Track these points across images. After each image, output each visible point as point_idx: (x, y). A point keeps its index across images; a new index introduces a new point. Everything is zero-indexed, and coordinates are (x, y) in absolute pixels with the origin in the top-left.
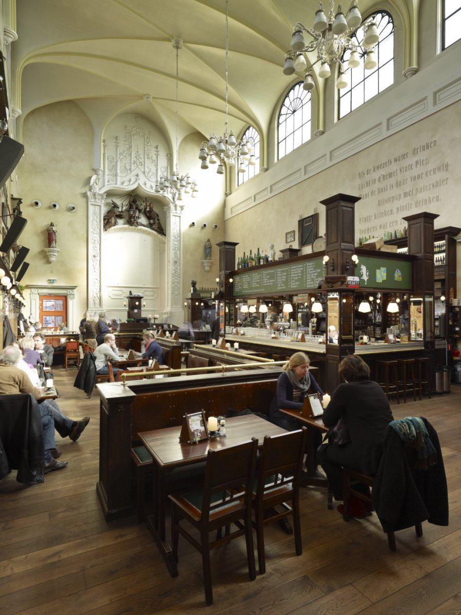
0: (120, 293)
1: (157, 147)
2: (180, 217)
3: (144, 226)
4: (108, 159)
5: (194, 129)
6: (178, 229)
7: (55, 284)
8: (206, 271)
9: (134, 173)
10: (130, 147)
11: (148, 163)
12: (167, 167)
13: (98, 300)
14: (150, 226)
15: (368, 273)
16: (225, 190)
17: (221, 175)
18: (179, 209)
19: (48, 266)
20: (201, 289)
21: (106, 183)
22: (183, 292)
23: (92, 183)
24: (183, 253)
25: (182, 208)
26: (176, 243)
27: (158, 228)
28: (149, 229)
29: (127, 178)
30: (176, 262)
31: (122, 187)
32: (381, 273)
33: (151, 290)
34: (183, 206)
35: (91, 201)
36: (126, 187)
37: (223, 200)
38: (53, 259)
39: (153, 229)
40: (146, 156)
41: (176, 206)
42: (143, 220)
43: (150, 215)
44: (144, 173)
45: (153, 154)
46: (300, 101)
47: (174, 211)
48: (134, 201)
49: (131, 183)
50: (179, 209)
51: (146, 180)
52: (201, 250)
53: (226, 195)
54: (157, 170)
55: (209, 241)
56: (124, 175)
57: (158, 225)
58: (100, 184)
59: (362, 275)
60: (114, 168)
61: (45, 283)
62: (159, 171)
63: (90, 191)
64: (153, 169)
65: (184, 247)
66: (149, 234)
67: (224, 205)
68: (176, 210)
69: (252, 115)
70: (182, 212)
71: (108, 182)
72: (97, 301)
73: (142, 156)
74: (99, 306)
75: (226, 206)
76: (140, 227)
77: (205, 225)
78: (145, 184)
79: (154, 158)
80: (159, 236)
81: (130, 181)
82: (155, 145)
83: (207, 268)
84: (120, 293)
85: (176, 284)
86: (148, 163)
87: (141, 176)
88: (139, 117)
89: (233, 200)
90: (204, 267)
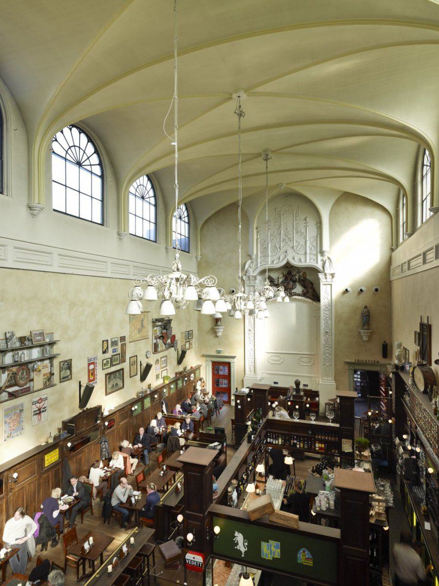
0: (278, 358)
1: (306, 219)
2: (331, 285)
3: (299, 295)
4: (260, 243)
5: (339, 191)
6: (330, 298)
7: (221, 354)
8: (364, 341)
9: (283, 250)
10: (280, 227)
11: (296, 237)
12: (317, 236)
13: (253, 367)
14: (304, 294)
15: (246, 544)
16: (391, 245)
17: (329, 257)
18: (329, 277)
19: (217, 339)
20: (357, 361)
21: (259, 265)
22: (335, 364)
23: (246, 268)
24: (335, 321)
25: (333, 275)
26: (326, 313)
27: (313, 296)
28: (303, 298)
29: (277, 256)
30: (327, 332)
31: (272, 265)
32: (269, 548)
33: (306, 356)
34: (334, 274)
35: (247, 282)
36: (276, 265)
37: (386, 259)
38: (220, 334)
39: (307, 297)
40: (294, 232)
41: (326, 275)
42: (299, 289)
43: (304, 282)
44: (293, 247)
45: (302, 224)
46: (142, 186)
47: (325, 280)
48: (289, 273)
49: (281, 260)
50: (329, 277)
51: (294, 254)
52: (357, 320)
53: (392, 250)
54: (306, 242)
55: (366, 307)
56: (274, 254)
57: (312, 293)
58: (253, 266)
59: (237, 544)
60: (265, 249)
61: (215, 354)
62: (308, 243)
63: (246, 275)
64: (302, 242)
65: (336, 316)
66: (305, 302)
67: (390, 262)
68: (326, 278)
69: (372, 170)
70: (333, 280)
71: (261, 263)
72: (252, 369)
73: (291, 232)
74: (253, 374)
75: (392, 263)
76: (294, 297)
77: (361, 290)
78: (294, 258)
79: (303, 230)
80: (314, 303)
81: (279, 258)
82: (303, 218)
83: (365, 338)
84: (278, 358)
85: (327, 355)
86: (296, 237)
87: (290, 251)
88: (287, 197)
89: (401, 256)
90: (362, 337)
